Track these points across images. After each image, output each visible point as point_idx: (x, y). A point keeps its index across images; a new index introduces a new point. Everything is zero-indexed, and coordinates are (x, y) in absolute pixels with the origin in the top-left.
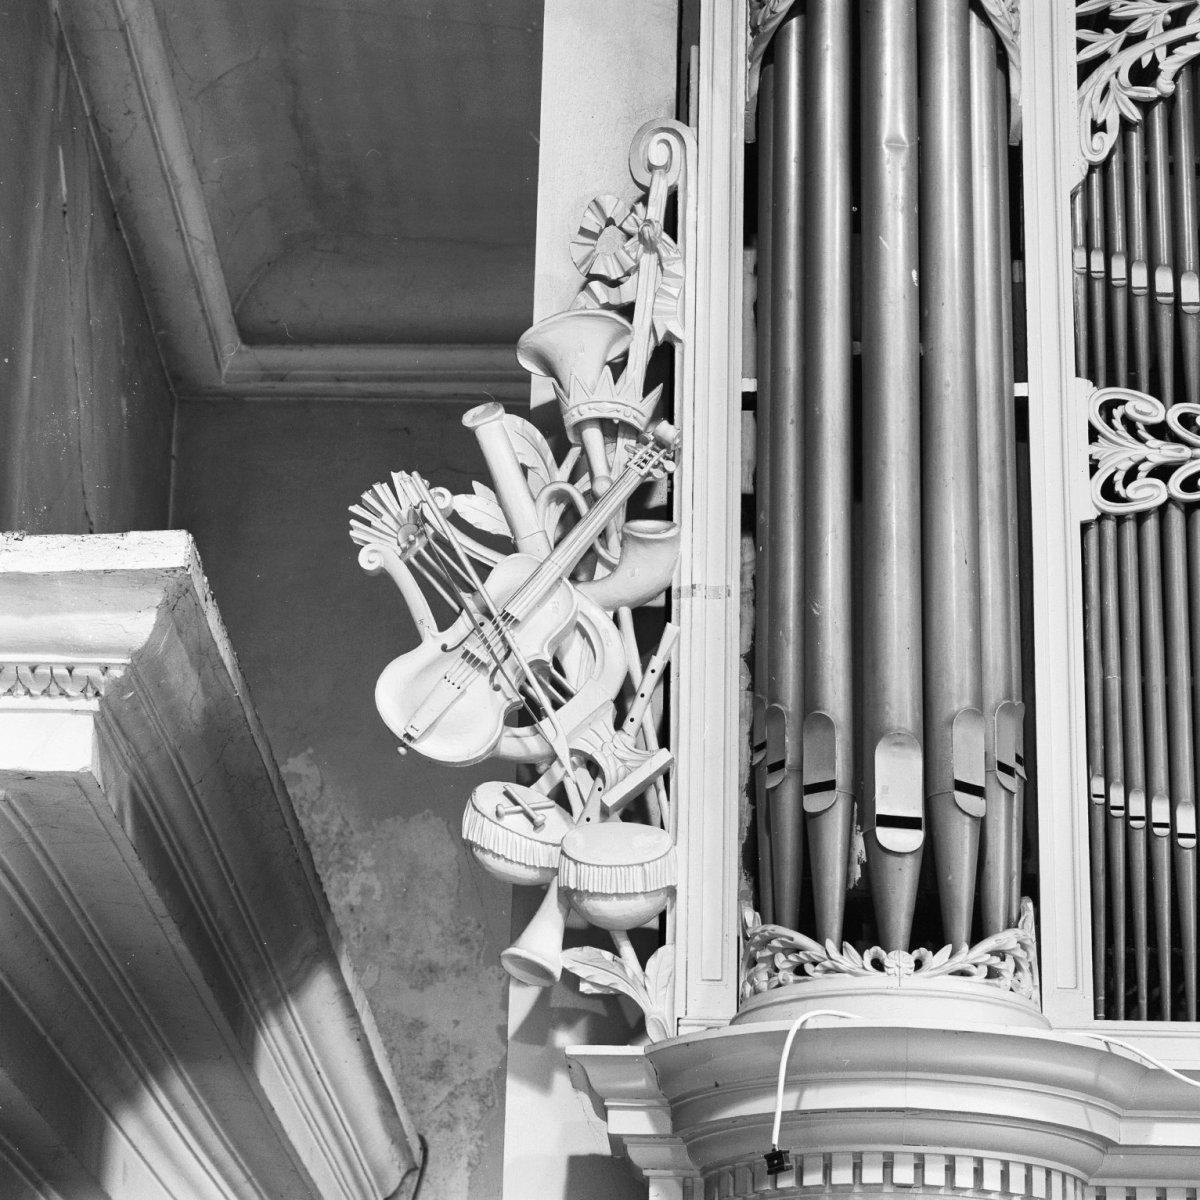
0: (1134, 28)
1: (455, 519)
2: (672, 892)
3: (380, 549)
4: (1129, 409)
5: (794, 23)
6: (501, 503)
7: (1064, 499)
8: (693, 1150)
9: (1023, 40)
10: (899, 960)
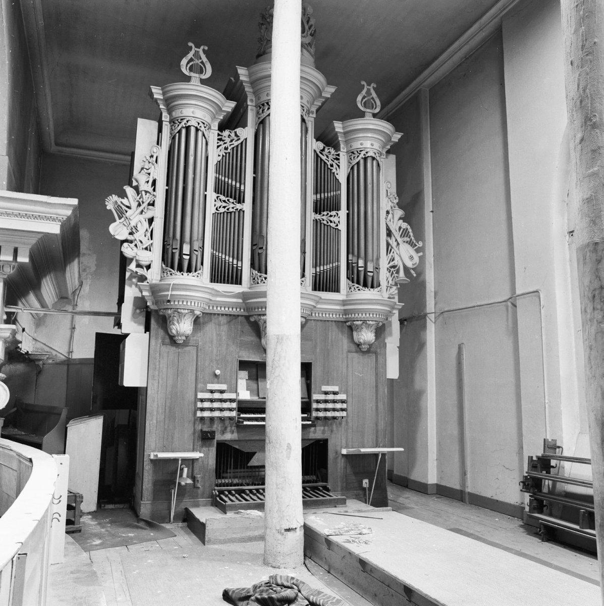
0: (225, 142)
1: (122, 203)
2: (152, 261)
3: (110, 206)
4: (220, 198)
5: (177, 134)
6: (129, 201)
7: (211, 210)
8: (154, 298)
9: (210, 138)
10: (185, 274)
